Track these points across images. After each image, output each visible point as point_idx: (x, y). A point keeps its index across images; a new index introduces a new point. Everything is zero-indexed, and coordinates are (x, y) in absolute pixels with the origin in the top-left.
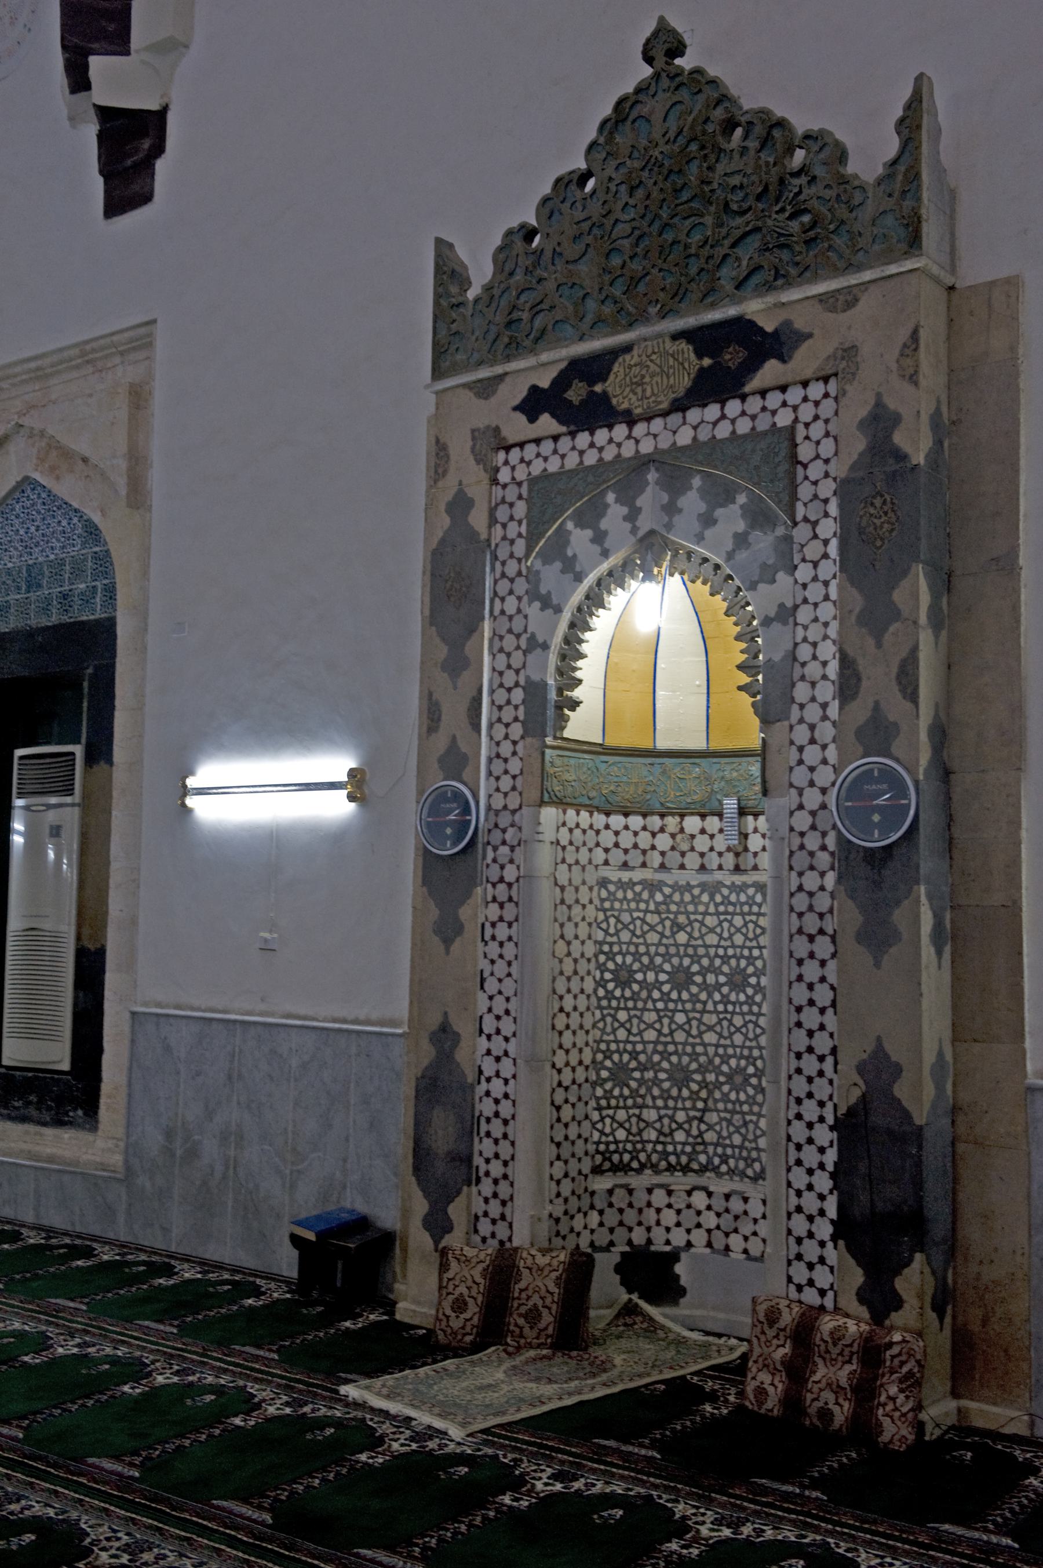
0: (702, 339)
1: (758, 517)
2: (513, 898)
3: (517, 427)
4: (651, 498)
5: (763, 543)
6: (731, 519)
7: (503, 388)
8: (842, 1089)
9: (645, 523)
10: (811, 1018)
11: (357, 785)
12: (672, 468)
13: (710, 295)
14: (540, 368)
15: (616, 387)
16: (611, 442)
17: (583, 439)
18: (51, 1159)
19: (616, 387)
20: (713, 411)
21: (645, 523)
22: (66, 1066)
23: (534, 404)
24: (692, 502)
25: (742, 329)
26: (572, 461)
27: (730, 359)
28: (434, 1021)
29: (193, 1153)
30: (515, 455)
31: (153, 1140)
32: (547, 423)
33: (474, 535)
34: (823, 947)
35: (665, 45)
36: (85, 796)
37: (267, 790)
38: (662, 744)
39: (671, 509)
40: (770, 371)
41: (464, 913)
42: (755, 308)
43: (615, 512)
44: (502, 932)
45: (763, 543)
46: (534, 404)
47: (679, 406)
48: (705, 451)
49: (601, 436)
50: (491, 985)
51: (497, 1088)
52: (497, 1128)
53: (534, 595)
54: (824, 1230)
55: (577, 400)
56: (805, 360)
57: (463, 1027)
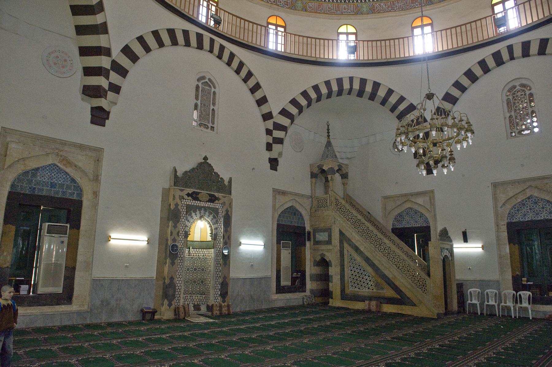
0: (210, 195)
1: (214, 217)
2: (182, 259)
3: (186, 197)
4: (202, 211)
5: (215, 220)
6: (193, 214)
7: (184, 191)
8: (220, 280)
9: (202, 214)
10: (218, 273)
11: (108, 238)
12: (205, 209)
13: (211, 190)
14: (190, 191)
15: (199, 196)
16: (197, 203)
17: (194, 201)
18: (62, 311)
19: (199, 196)
20: (210, 204)
21: (202, 214)
22: (61, 292)
23: (188, 195)
24: (207, 213)
25: (213, 196)
26: (193, 204)
27: (213, 199)
28: (170, 276)
29: (108, 304)
30: (184, 200)
31: (98, 303)
32: (190, 198)
33: (179, 210)
34: (219, 265)
35: (206, 158)
36: (69, 235)
37: (129, 240)
38: (195, 240)
39: (205, 214)
40: (217, 201)
41: (176, 261)
42: (216, 194)
43: (198, 212)
44: (180, 264)
45: (215, 220)
46: (188, 195)
47: (206, 202)
48: (209, 208)
49: (196, 202)
50: (178, 271)
51: (179, 285)
52: (178, 290)
53: (187, 220)
54: (218, 295)
55: (194, 196)
56: (221, 202)
57: (175, 277)
